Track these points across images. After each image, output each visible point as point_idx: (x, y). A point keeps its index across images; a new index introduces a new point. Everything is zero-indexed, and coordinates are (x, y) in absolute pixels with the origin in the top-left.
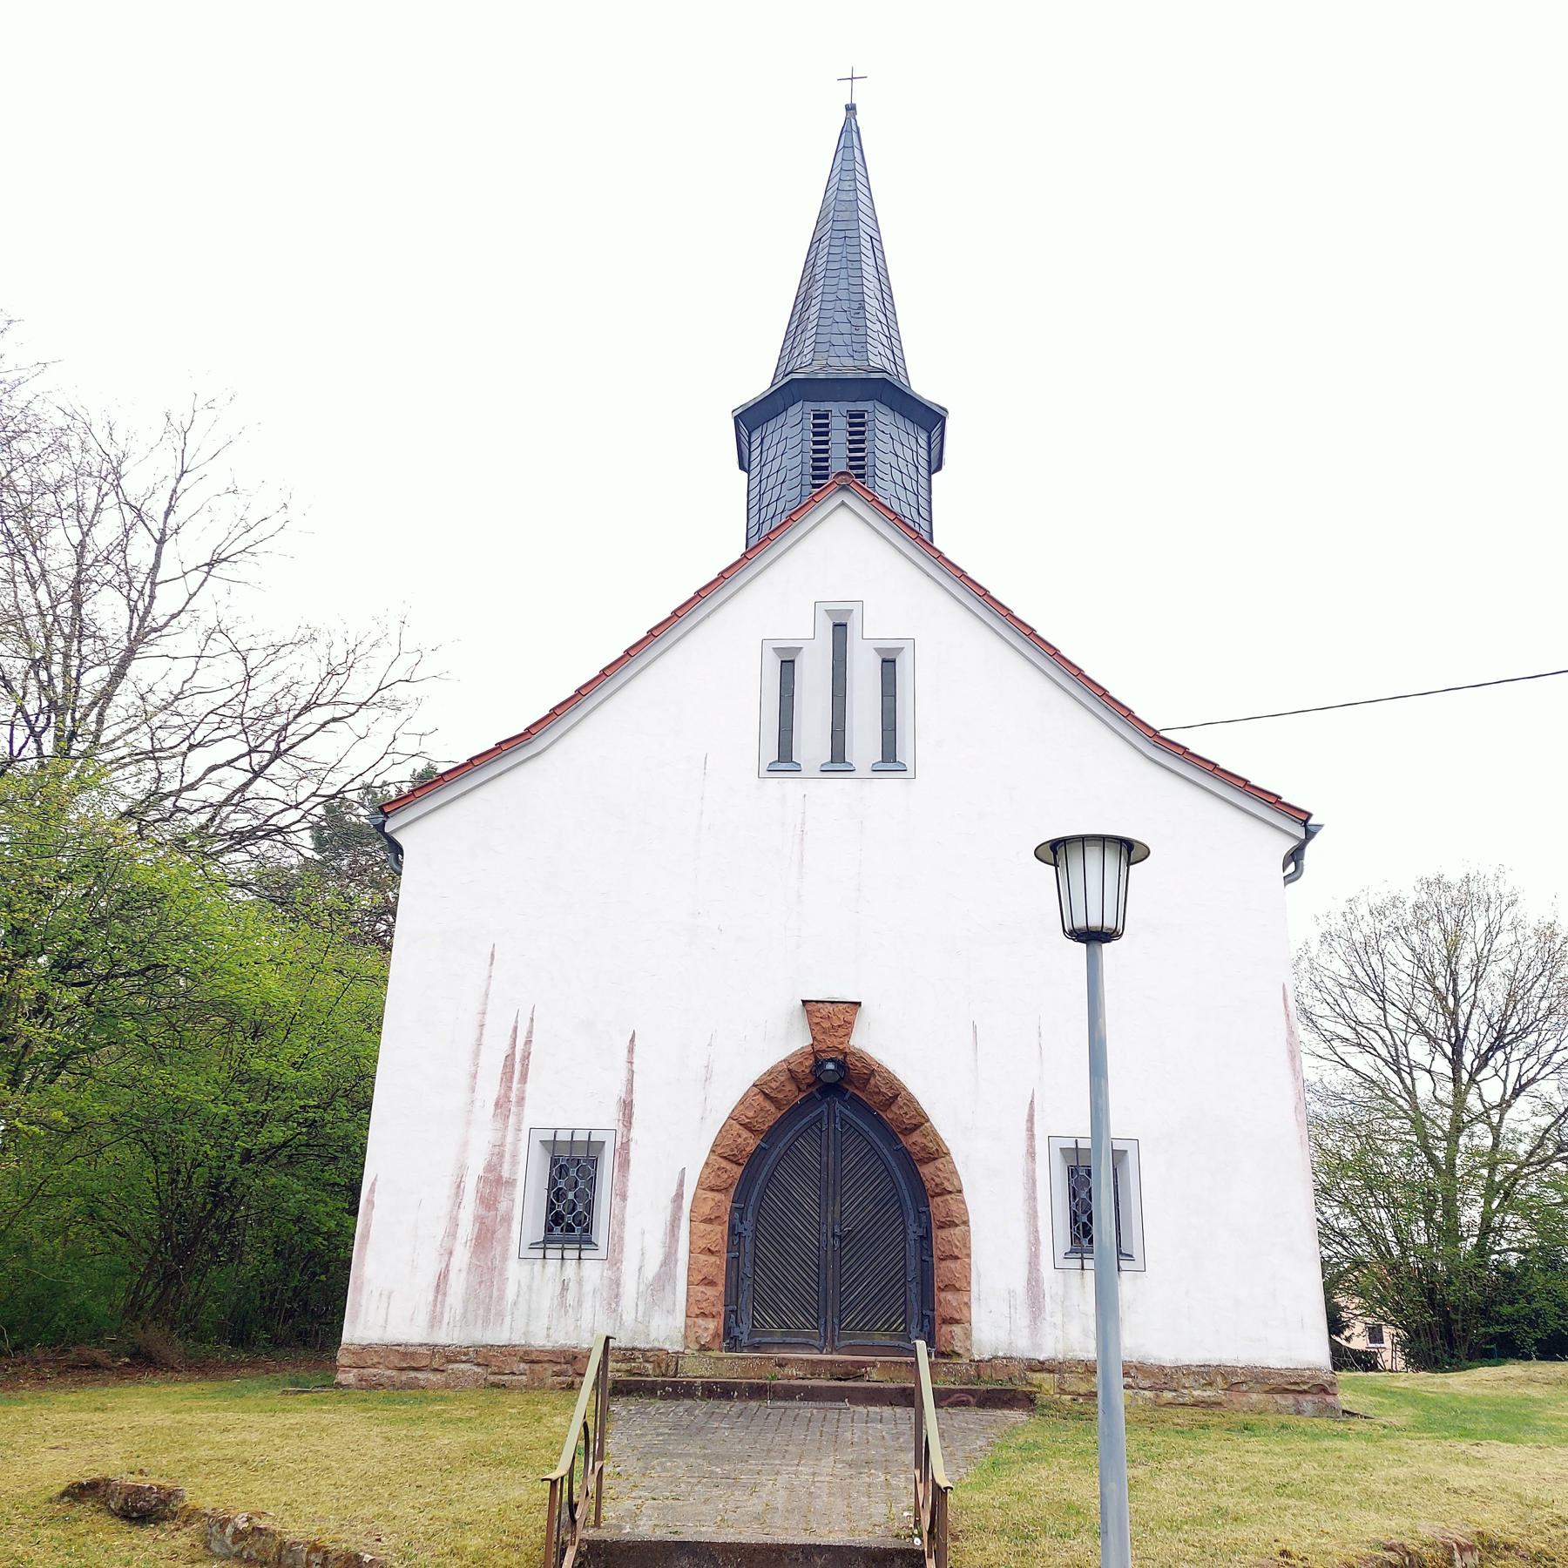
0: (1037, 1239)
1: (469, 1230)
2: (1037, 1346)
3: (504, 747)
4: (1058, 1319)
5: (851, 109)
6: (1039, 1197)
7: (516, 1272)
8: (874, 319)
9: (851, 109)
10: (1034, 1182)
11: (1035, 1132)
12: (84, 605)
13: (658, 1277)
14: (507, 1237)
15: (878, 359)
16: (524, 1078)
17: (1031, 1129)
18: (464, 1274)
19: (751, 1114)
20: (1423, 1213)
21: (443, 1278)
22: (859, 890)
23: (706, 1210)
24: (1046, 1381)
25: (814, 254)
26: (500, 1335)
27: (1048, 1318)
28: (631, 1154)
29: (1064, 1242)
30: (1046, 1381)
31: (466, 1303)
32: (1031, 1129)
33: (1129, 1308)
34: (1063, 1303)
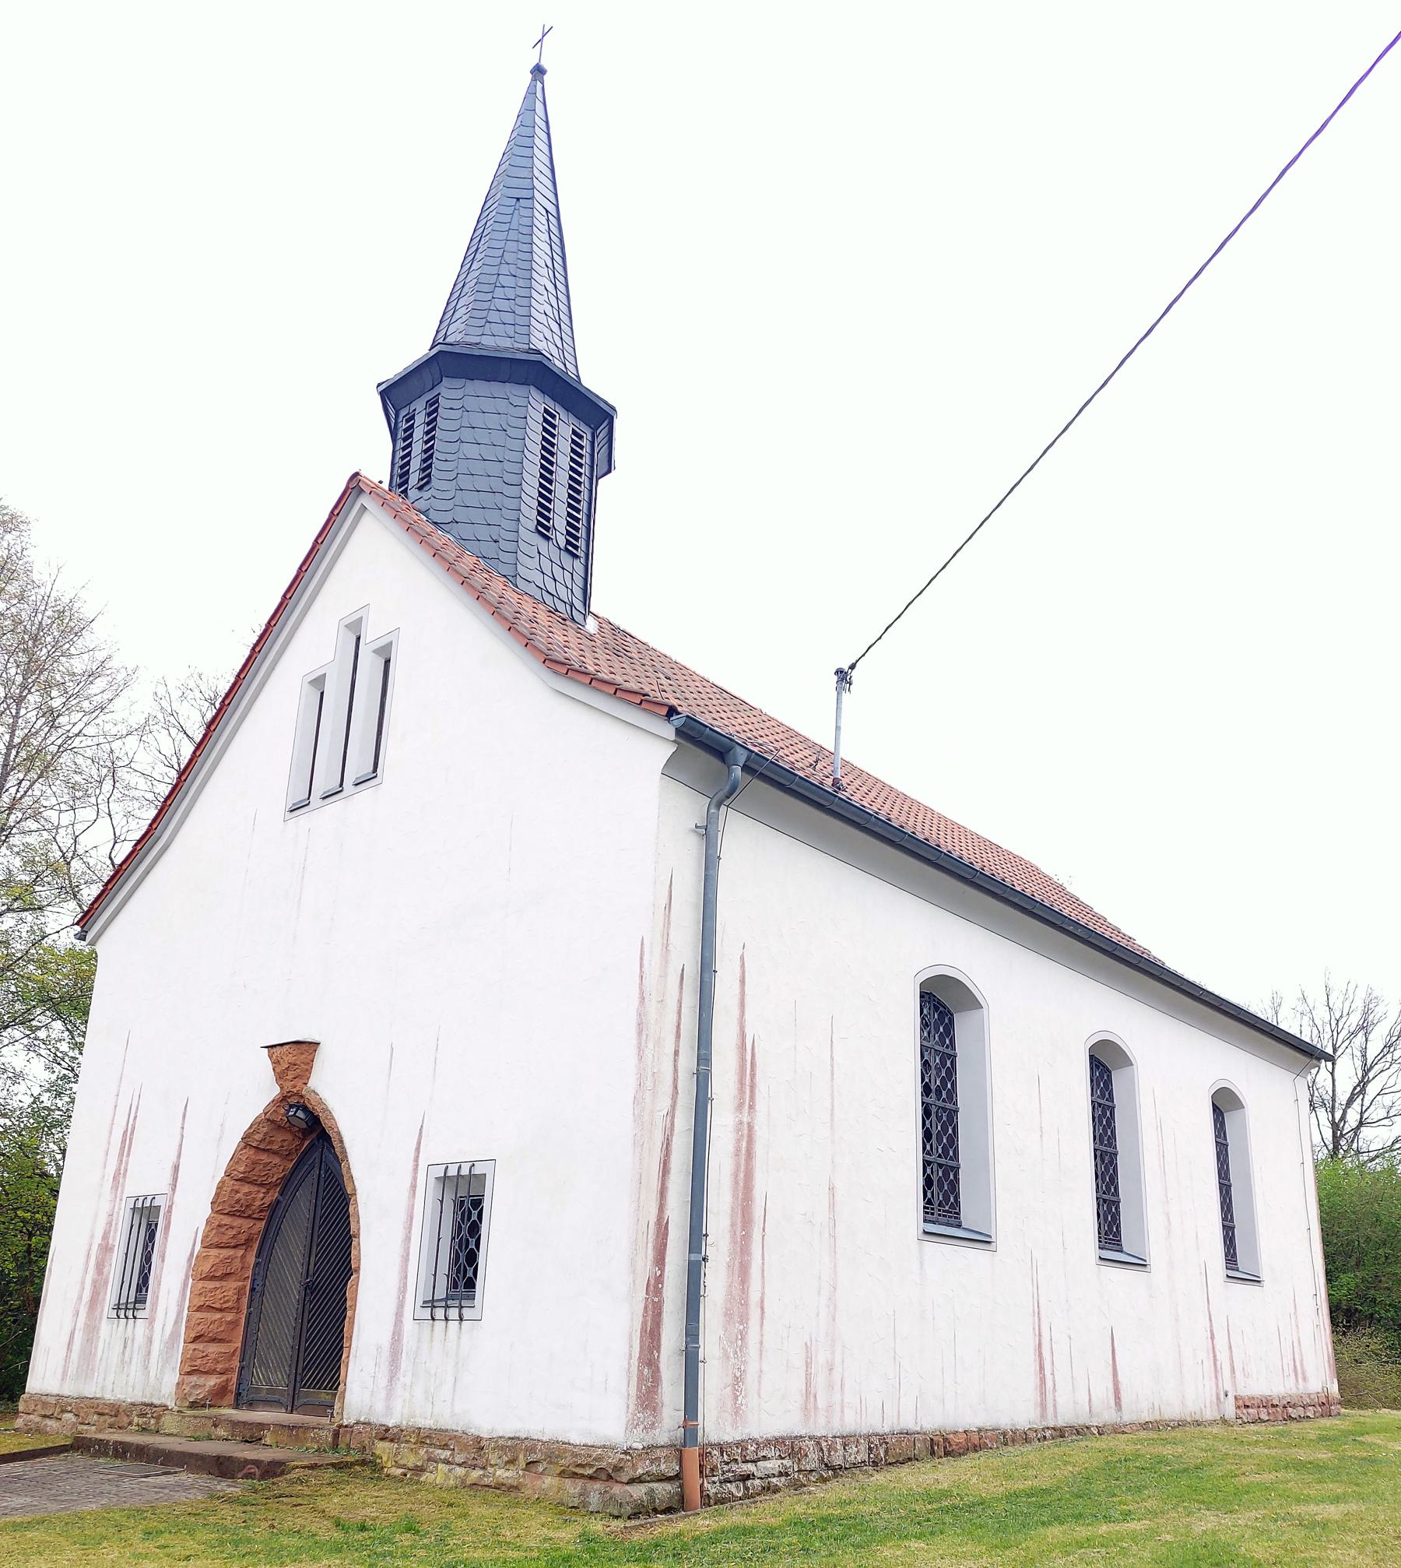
0: (405, 1284)
1: (652, 1255)
2: (389, 1409)
3: (139, 847)
4: (408, 1380)
5: (539, 71)
6: (412, 1239)
7: (105, 1328)
8: (541, 290)
9: (539, 71)
10: (412, 1218)
11: (420, 1163)
12: (689, 807)
13: (172, 1334)
14: (104, 1299)
15: (543, 340)
16: (128, 1155)
17: (416, 1159)
18: (81, 1332)
19: (242, 1169)
20: (36, 1276)
21: (72, 1334)
22: (332, 919)
23: (206, 1267)
24: (382, 1448)
25: (475, 248)
26: (90, 1390)
27: (401, 1378)
28: (172, 1217)
29: (418, 1285)
30: (382, 1448)
31: (79, 1358)
32: (416, 1159)
33: (463, 1365)
34: (414, 1359)
